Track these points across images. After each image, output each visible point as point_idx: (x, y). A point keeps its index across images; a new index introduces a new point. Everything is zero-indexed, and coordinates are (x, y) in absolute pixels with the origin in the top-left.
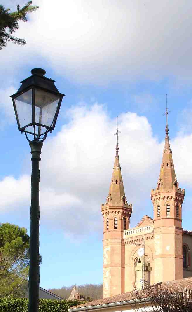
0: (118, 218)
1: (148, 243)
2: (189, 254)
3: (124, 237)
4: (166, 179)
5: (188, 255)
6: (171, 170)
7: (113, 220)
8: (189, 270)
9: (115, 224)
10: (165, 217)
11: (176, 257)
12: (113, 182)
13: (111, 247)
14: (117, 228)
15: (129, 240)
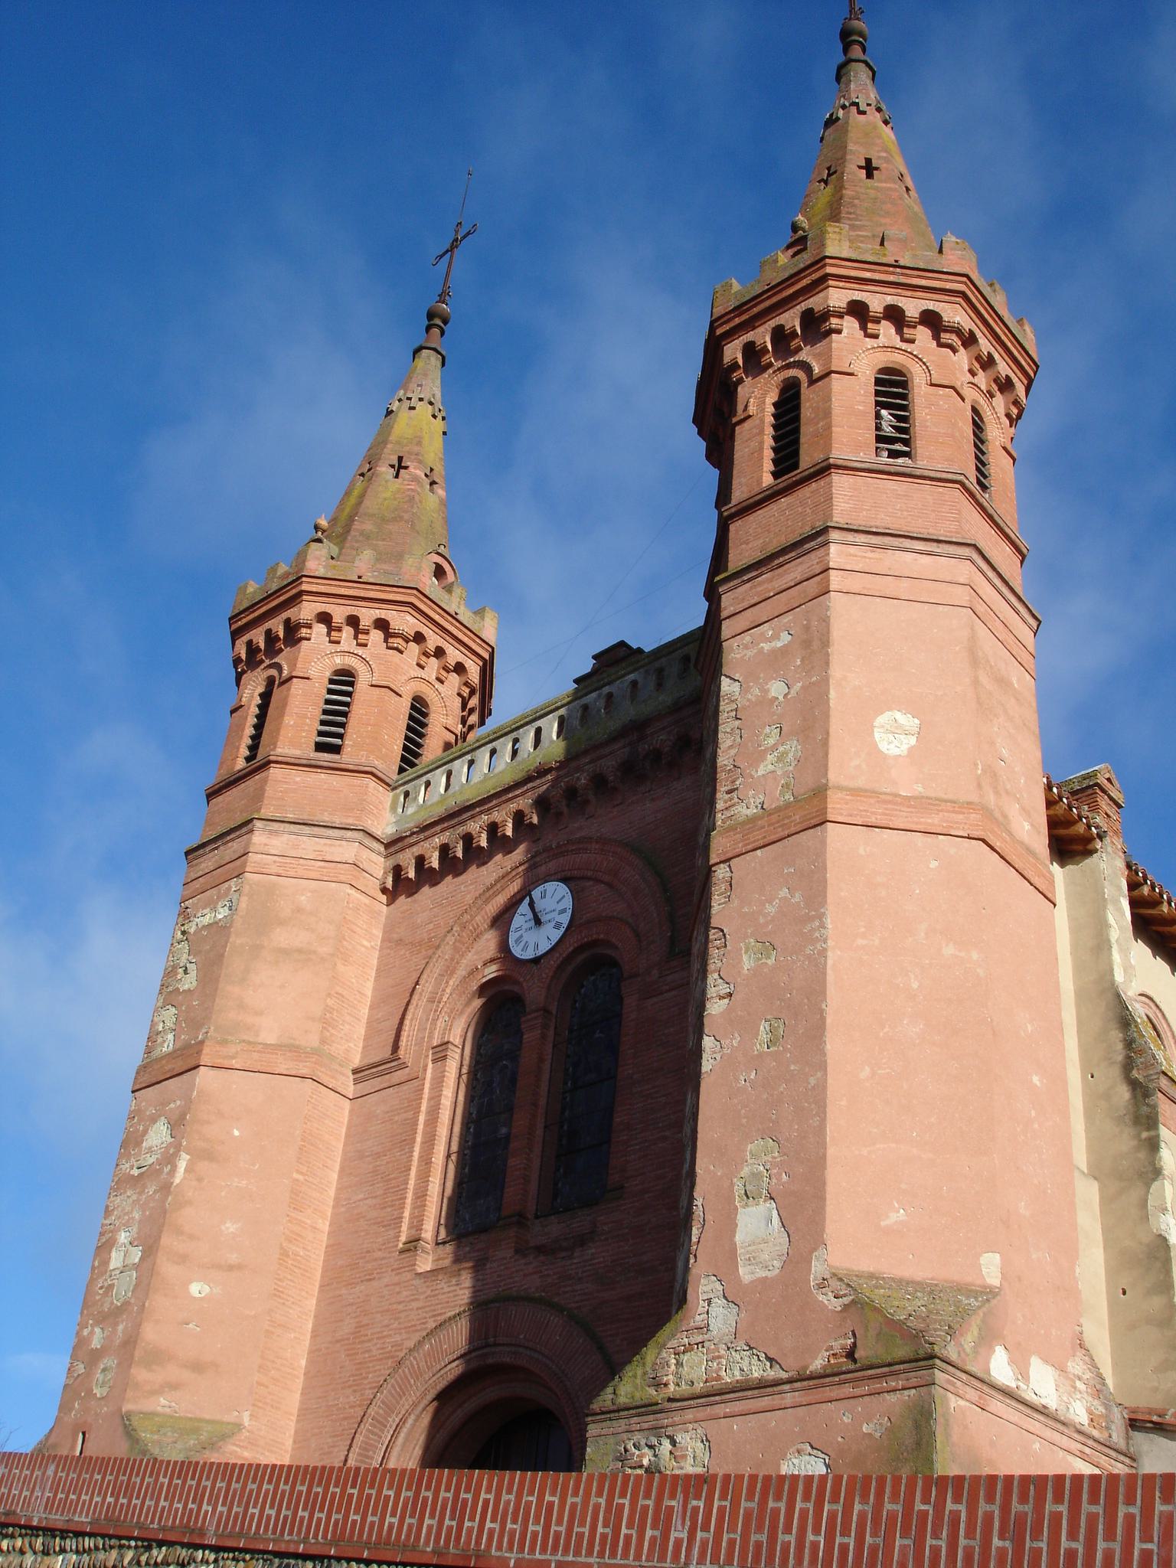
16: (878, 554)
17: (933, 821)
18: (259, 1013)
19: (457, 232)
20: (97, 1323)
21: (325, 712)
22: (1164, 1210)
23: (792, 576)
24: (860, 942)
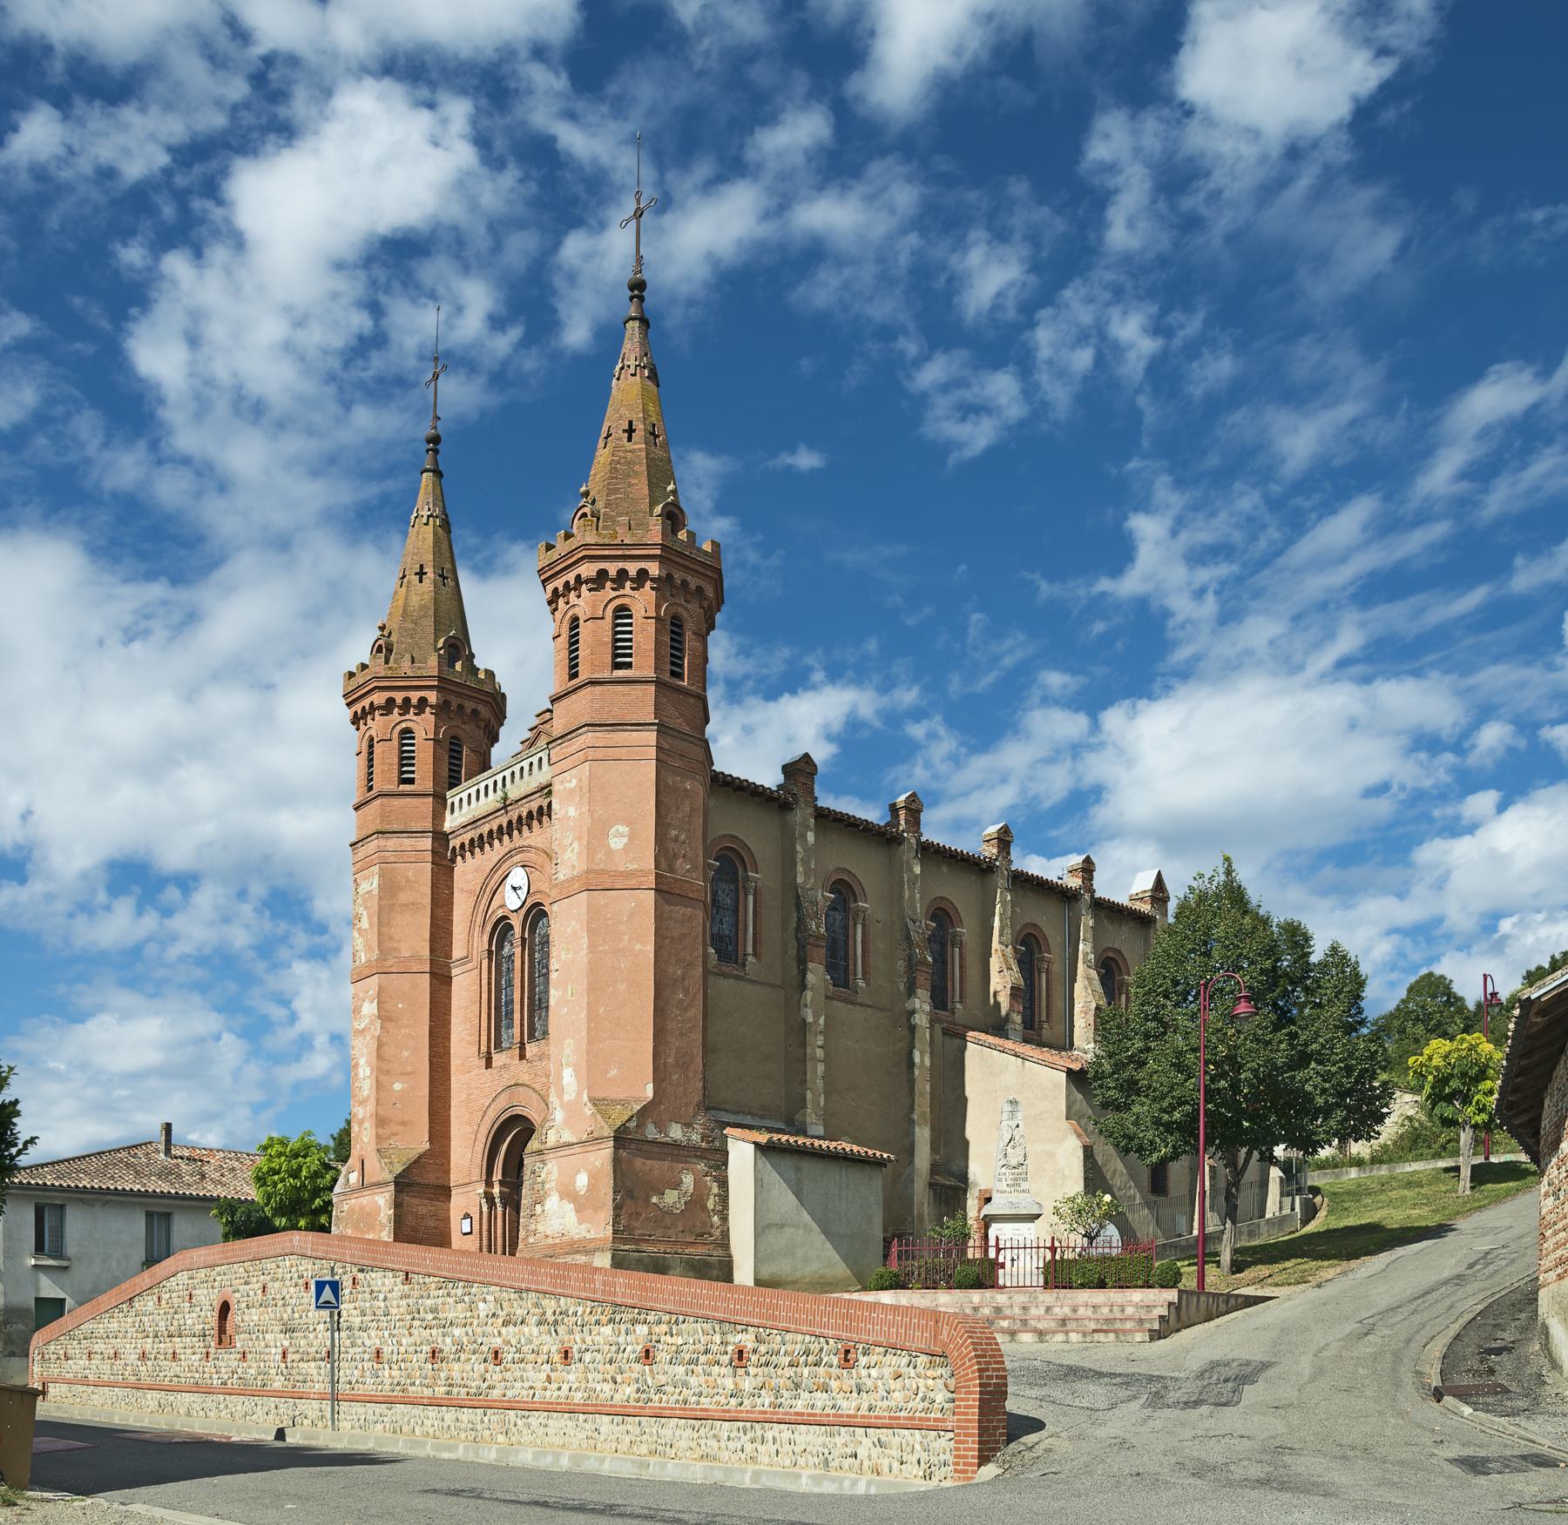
0: (420, 734)
1: (533, 837)
2: (755, 895)
3: (450, 822)
4: (617, 491)
5: (751, 898)
6: (648, 454)
7: (395, 743)
8: (751, 976)
9: (405, 759)
10: (606, 674)
11: (666, 891)
12: (404, 577)
13: (382, 875)
14: (411, 781)
15: (466, 838)
16: (611, 735)
17: (633, 883)
18: (399, 941)
19: (638, 202)
20: (359, 1105)
21: (413, 758)
22: (806, 1006)
23: (574, 747)
24: (600, 948)
